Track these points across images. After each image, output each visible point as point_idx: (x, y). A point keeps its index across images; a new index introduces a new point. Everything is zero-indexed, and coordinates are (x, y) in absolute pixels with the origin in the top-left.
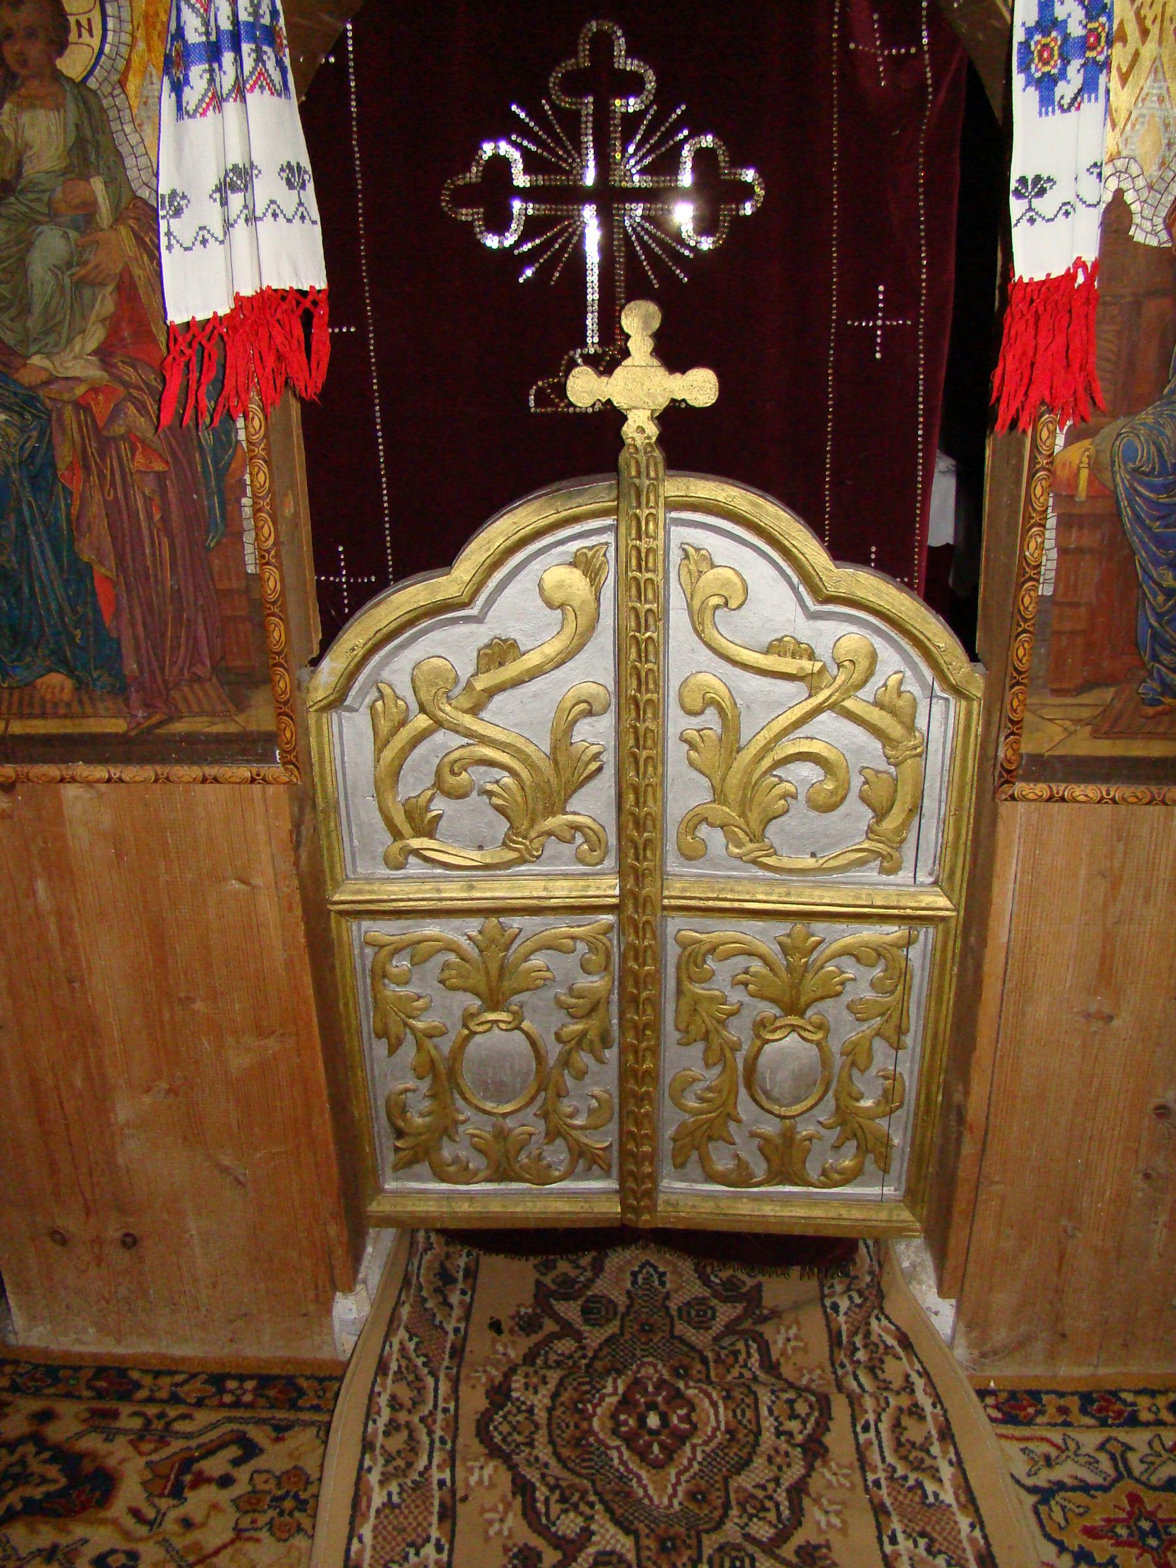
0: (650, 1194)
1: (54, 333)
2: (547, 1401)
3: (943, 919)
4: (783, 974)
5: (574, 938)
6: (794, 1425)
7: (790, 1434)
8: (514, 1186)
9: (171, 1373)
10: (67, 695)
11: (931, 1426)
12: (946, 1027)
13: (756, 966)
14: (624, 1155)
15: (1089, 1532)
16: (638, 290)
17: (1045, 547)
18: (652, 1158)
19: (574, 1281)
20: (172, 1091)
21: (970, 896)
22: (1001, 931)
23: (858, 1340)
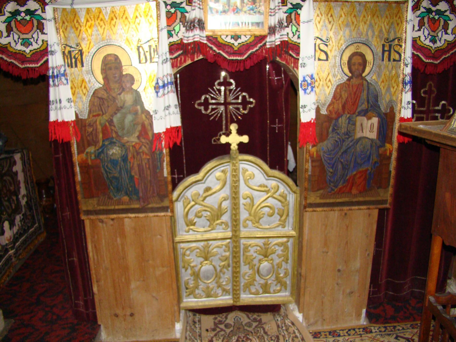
0: (239, 298)
1: (129, 133)
3: (295, 236)
4: (264, 249)
5: (222, 245)
8: (211, 299)
10: (127, 201)
11: (300, 339)
12: (296, 258)
13: (258, 248)
14: (234, 290)
16: (232, 121)
17: (309, 166)
18: (239, 290)
20: (144, 280)
21: (299, 231)
22: (306, 237)
23: (283, 325)
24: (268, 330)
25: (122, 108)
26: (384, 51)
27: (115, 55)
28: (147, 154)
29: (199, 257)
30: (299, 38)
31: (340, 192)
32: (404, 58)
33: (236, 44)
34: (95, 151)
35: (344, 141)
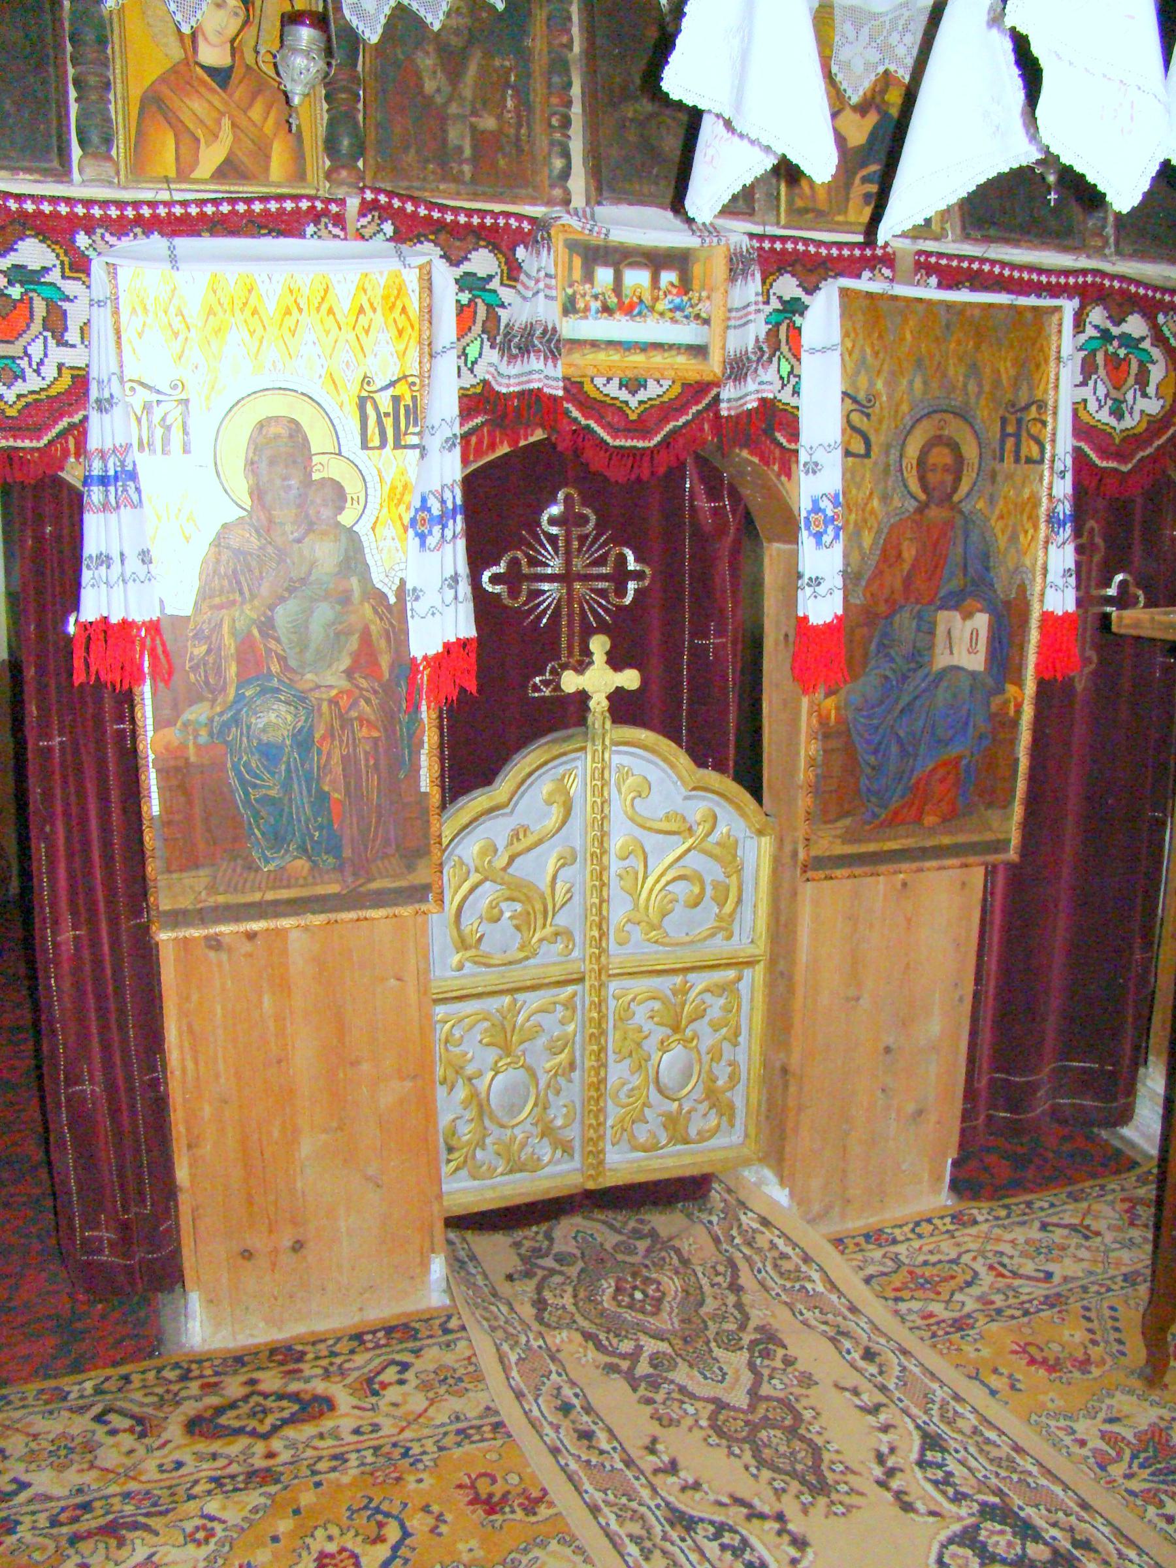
0: (601, 1163)
2: (572, 1300)
6: (719, 1279)
7: (718, 1284)
9: (325, 1340)
15: (896, 1290)
19: (540, 1249)
23: (734, 1232)
24: (690, 1252)
25: (303, 581)
26: (1004, 436)
27: (293, 421)
28: (371, 725)
29: (488, 1045)
30: (796, 392)
31: (895, 820)
32: (1053, 456)
33: (633, 402)
34: (211, 720)
35: (905, 678)
